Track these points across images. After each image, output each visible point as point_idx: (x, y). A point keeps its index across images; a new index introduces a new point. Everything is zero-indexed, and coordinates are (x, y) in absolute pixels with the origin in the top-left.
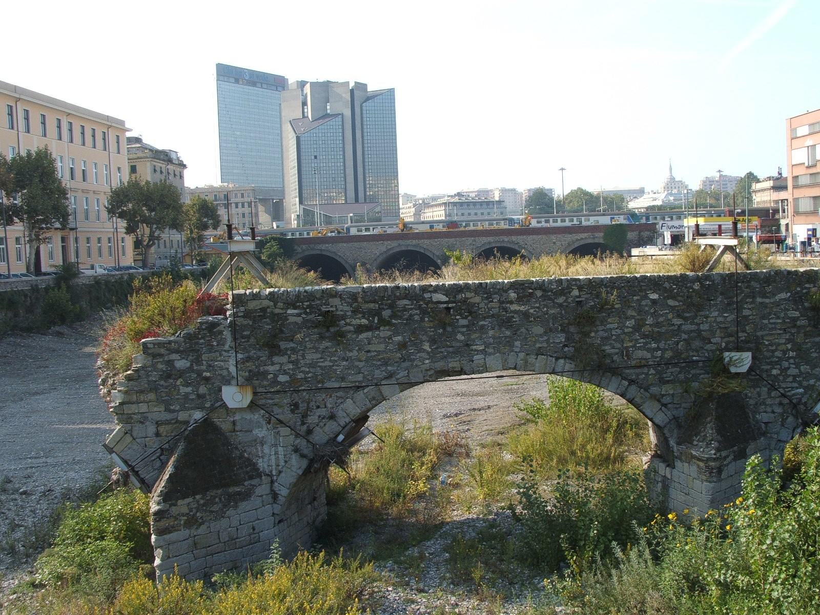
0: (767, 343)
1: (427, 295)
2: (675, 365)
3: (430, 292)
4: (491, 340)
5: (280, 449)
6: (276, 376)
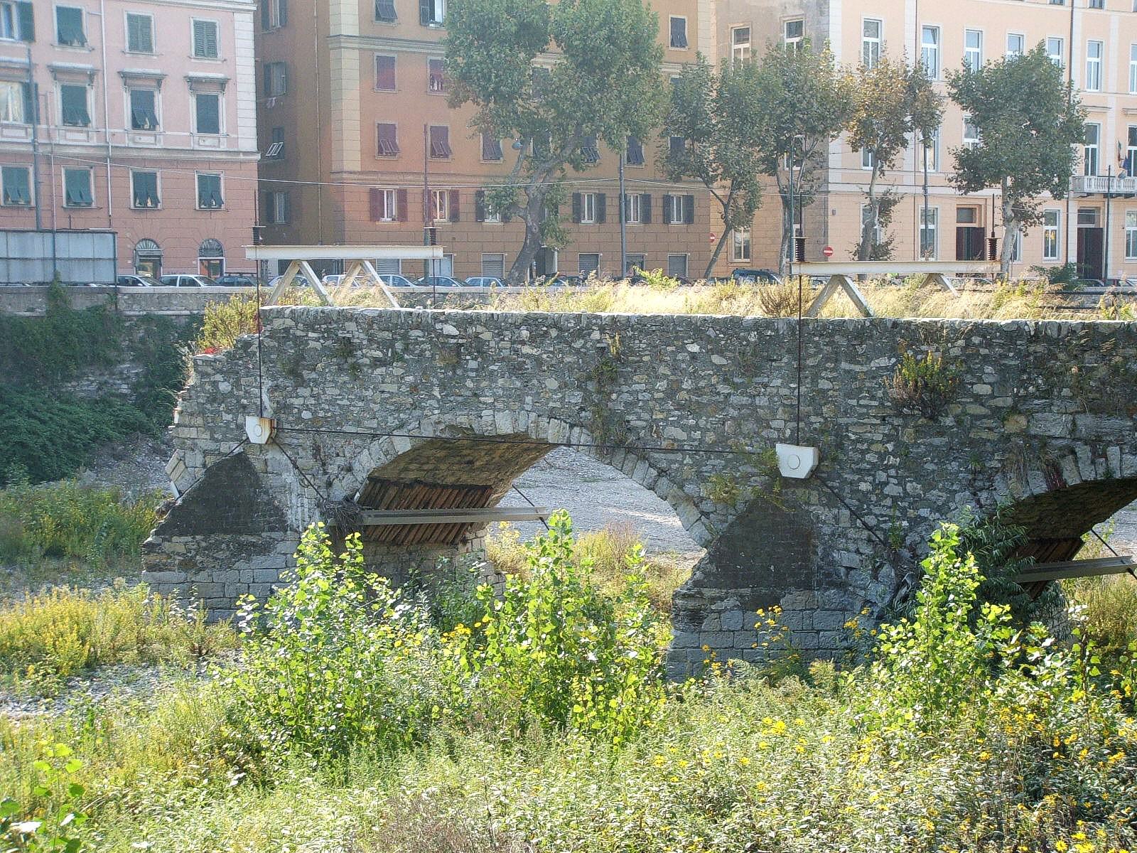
0: (853, 437)
1: (438, 326)
2: (720, 454)
3: (441, 322)
4: (501, 392)
5: (306, 501)
6: (300, 412)
